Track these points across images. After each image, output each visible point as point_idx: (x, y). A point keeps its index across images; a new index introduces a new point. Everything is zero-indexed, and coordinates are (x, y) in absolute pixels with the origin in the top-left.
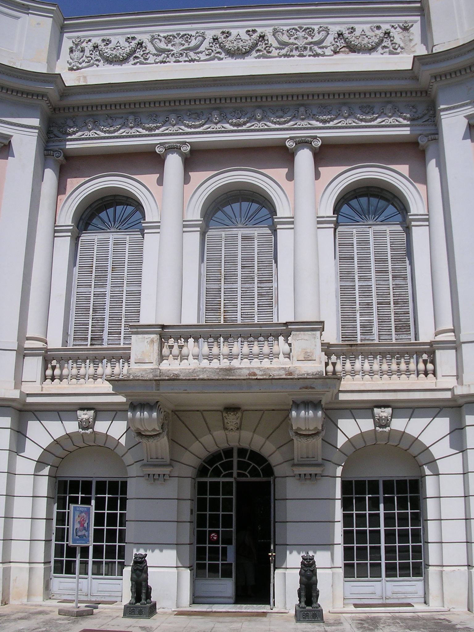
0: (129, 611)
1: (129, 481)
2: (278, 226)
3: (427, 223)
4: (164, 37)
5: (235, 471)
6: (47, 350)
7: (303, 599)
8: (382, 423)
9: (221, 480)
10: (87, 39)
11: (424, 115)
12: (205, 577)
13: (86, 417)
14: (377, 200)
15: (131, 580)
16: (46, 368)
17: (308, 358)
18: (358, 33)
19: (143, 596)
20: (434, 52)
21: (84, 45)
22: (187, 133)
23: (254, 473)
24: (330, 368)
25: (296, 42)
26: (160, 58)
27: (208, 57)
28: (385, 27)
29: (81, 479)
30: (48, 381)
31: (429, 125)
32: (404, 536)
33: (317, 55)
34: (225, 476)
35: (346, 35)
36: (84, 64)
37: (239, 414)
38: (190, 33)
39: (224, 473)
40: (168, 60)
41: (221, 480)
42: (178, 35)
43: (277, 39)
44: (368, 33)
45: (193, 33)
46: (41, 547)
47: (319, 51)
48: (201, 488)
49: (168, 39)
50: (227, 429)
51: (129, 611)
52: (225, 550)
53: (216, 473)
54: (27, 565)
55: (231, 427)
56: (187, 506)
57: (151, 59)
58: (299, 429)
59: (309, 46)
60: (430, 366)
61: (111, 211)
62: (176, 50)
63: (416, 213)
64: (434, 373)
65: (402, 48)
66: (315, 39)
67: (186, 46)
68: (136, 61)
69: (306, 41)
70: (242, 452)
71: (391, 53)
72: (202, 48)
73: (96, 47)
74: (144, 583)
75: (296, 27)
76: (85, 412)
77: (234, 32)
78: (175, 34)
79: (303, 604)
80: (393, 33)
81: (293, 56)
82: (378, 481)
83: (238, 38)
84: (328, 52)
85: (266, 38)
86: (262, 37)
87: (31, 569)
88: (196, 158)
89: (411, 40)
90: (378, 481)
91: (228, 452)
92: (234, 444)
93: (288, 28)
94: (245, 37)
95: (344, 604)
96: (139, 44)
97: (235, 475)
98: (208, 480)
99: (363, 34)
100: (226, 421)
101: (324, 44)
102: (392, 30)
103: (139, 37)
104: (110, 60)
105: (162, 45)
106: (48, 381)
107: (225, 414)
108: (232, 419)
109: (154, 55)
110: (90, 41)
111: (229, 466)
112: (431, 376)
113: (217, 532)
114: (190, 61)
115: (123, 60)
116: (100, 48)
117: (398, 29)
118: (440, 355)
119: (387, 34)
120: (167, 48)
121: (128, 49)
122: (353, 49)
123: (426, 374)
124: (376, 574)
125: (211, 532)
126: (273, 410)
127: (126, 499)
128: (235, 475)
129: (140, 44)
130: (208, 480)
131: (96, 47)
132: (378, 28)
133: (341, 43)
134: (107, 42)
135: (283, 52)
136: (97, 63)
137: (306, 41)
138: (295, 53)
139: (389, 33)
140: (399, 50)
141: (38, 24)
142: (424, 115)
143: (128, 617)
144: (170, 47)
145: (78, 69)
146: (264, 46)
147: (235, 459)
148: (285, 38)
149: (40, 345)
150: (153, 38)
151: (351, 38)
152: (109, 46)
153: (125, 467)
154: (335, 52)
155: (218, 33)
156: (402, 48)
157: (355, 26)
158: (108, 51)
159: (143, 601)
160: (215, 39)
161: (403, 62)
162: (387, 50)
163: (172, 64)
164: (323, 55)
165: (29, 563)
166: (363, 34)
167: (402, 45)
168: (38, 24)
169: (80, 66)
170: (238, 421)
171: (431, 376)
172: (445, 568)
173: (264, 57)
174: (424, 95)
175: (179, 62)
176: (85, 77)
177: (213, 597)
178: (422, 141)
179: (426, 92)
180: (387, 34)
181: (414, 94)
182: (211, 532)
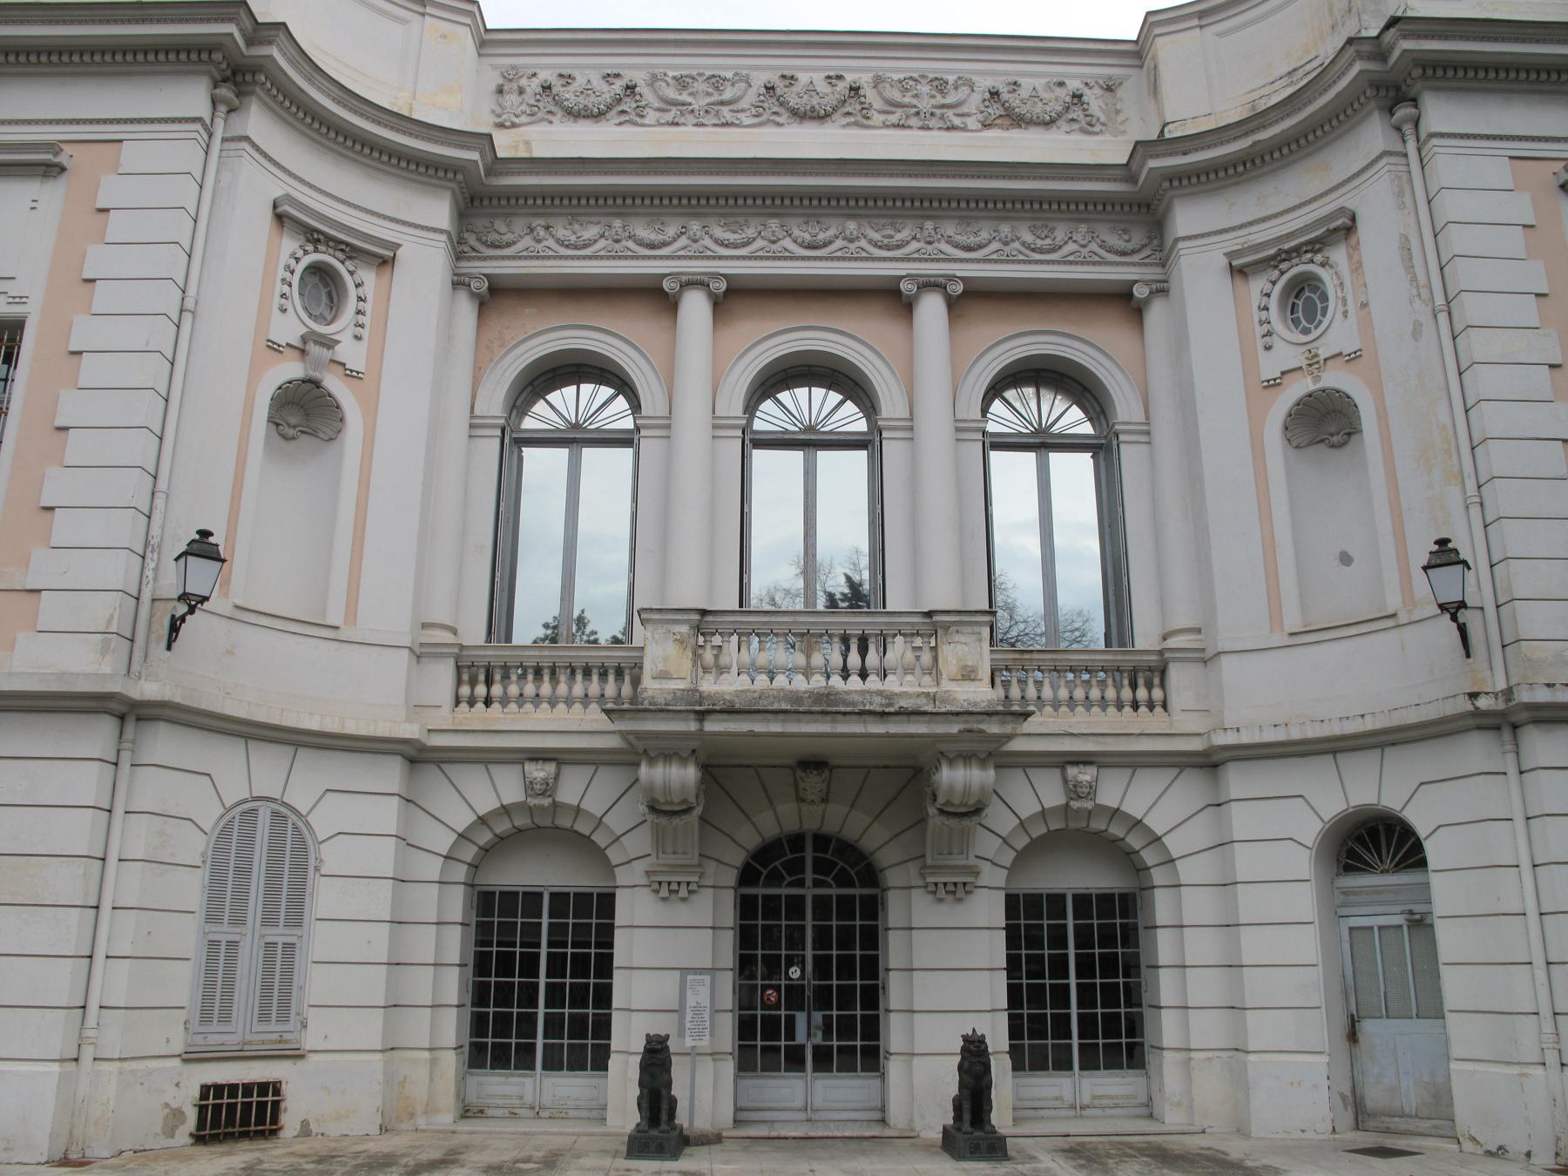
0: (640, 1146)
1: (618, 892)
2: (1122, 437)
3: (1143, 438)
4: (674, 78)
5: (809, 876)
6: (462, 647)
7: (967, 1117)
8: (1074, 790)
9: (784, 891)
10: (530, 72)
11: (1143, 246)
12: (755, 1070)
13: (542, 774)
14: (824, 391)
15: (641, 1084)
16: (459, 682)
17: (968, 675)
18: (1024, 92)
19: (664, 1117)
20: (1167, 136)
21: (524, 82)
22: (721, 258)
23: (844, 880)
24: (1000, 692)
25: (915, 102)
26: (668, 117)
27: (756, 120)
28: (1074, 85)
29: (521, 890)
30: (464, 706)
31: (1151, 265)
32: (846, 939)
33: (952, 128)
34: (791, 885)
35: (1005, 96)
36: (524, 119)
37: (826, 773)
38: (723, 74)
39: (788, 879)
40: (682, 120)
41: (784, 891)
42: (700, 75)
43: (880, 94)
44: (1046, 95)
45: (729, 75)
46: (451, 1016)
47: (957, 121)
48: (746, 907)
49: (682, 83)
50: (803, 801)
51: (640, 1146)
52: (791, 1021)
53: (774, 879)
54: (426, 1055)
55: (811, 798)
56: (728, 940)
57: (651, 116)
58: (948, 803)
59: (938, 112)
60: (1157, 694)
61: (835, 397)
62: (699, 103)
63: (1127, 419)
64: (1165, 706)
65: (1103, 124)
66: (948, 100)
67: (716, 98)
68: (622, 118)
69: (933, 102)
70: (822, 841)
71: (1083, 131)
72: (744, 104)
73: (547, 88)
74: (664, 1092)
75: (915, 75)
76: (540, 765)
77: (803, 78)
78: (694, 73)
79: (967, 1126)
80: (1090, 96)
81: (910, 127)
82: (1063, 896)
83: (811, 89)
84: (972, 123)
85: (861, 92)
86: (855, 90)
87: (434, 1061)
88: (971, 300)
89: (1118, 112)
90: (1063, 896)
91: (796, 841)
92: (811, 825)
93: (902, 76)
94: (822, 87)
95: (1014, 1119)
96: (628, 87)
97: (809, 882)
98: (760, 891)
99: (1035, 95)
100: (802, 785)
101: (964, 109)
102: (1086, 91)
103: (630, 76)
104: (575, 114)
105: (672, 94)
106: (464, 706)
107: (799, 773)
108: (813, 783)
109: (658, 110)
110: (534, 75)
111: (796, 867)
112: (1158, 709)
113: (777, 988)
114: (723, 125)
115: (598, 116)
116: (555, 90)
117: (1097, 91)
118: (1175, 674)
119: (1077, 97)
120: (680, 98)
121: (607, 96)
122: (1016, 120)
123: (1151, 706)
124: (1064, 1064)
125: (764, 988)
126: (886, 767)
127: (611, 928)
128: (809, 882)
129: (631, 88)
130: (760, 891)
131: (547, 88)
132: (1061, 84)
133: (995, 110)
134: (567, 79)
135: (893, 119)
136: (550, 117)
137: (933, 102)
138: (913, 122)
139: (1080, 96)
140: (1096, 129)
141: (444, 36)
142: (1143, 246)
143: (638, 1158)
144: (685, 97)
145: (514, 125)
146: (859, 107)
147: (809, 855)
148: (895, 95)
149: (447, 637)
150: (654, 79)
151: (1013, 100)
152: (571, 88)
153: (609, 868)
154: (986, 126)
155: (773, 78)
156: (1103, 124)
157: (1021, 80)
158: (569, 95)
159: (664, 1126)
160: (770, 89)
161: (1111, 150)
162: (1076, 126)
163: (691, 129)
164: (965, 129)
165: (430, 1049)
166: (1035, 95)
167: (1103, 118)
168: (444, 36)
169: (517, 121)
170: (824, 786)
171: (1158, 709)
172: (1193, 1054)
173: (856, 124)
174: (1144, 210)
175: (703, 125)
176: (528, 143)
177: (784, 1110)
178: (1140, 292)
179: (1148, 206)
180: (1077, 97)
181: (1126, 208)
182: (764, 988)
